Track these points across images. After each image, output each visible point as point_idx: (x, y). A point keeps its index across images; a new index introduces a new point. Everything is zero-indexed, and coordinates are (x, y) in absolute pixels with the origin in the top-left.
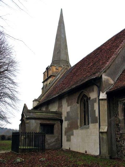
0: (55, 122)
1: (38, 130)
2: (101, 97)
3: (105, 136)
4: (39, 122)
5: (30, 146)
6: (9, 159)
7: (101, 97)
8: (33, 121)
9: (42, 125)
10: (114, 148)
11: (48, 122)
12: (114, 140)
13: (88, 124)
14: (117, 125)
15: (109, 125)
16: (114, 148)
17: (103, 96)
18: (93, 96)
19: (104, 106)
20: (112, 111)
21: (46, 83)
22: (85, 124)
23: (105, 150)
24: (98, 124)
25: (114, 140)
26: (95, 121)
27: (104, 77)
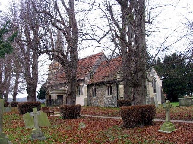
0: (64, 94)
1: (57, 98)
2: (84, 86)
3: (86, 99)
4: (57, 94)
5: (129, 105)
6: (16, 118)
7: (84, 86)
8: (54, 94)
9: (58, 96)
10: (89, 103)
11: (61, 94)
12: (89, 100)
13: (79, 95)
14: (90, 95)
15: (87, 95)
16: (89, 103)
17: (85, 85)
18: (81, 84)
19: (86, 89)
20: (88, 91)
21: (51, 72)
22: (78, 95)
23: (86, 104)
24: (83, 95)
25: (89, 100)
26: (82, 94)
27: (86, 79)
